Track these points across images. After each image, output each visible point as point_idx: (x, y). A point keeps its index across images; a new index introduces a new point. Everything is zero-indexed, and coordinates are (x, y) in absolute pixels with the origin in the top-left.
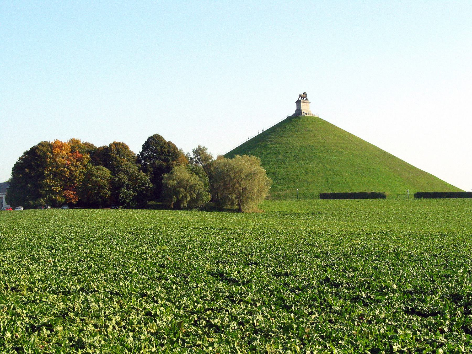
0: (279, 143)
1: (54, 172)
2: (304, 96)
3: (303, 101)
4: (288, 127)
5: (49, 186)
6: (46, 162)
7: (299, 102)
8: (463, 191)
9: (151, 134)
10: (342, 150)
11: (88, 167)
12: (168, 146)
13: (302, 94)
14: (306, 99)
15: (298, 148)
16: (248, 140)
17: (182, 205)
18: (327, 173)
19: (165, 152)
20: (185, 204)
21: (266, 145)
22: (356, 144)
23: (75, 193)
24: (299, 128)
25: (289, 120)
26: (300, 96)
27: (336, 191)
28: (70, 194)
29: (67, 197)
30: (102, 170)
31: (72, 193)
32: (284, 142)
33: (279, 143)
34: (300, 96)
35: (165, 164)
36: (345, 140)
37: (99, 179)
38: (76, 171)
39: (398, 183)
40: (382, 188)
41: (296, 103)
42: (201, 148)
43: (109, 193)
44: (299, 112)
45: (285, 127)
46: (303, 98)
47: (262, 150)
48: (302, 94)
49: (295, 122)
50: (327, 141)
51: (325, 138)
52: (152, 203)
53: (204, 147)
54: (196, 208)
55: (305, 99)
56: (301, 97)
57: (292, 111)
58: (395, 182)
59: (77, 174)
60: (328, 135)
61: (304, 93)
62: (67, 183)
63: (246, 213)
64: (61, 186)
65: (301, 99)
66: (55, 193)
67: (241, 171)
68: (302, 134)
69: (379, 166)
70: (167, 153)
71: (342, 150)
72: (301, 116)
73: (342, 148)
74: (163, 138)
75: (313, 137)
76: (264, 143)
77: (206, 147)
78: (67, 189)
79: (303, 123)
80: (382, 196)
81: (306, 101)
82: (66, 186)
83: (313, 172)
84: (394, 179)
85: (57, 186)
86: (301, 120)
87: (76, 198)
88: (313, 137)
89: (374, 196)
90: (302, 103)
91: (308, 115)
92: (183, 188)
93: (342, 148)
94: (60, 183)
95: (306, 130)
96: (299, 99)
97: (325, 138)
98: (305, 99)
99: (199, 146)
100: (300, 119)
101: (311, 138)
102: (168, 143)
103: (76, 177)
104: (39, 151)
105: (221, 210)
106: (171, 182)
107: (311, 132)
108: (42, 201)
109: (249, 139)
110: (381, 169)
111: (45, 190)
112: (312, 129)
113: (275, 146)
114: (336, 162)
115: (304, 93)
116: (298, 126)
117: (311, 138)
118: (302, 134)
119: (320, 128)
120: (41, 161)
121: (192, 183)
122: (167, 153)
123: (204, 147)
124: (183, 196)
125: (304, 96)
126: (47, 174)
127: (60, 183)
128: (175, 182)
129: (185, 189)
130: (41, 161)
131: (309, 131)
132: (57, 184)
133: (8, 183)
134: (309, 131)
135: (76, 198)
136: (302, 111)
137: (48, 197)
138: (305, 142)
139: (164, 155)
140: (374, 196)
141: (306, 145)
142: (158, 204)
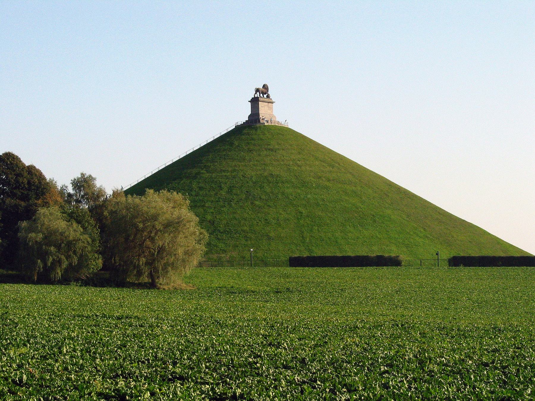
0: (221, 171)
2: (264, 90)
4: (236, 143)
7: (255, 102)
10: (328, 184)
12: (29, 174)
13: (261, 87)
14: (268, 97)
15: (254, 179)
17: (52, 276)
18: (302, 222)
19: (22, 183)
20: (59, 273)
21: (198, 173)
22: (351, 173)
24: (254, 145)
26: (257, 90)
27: (318, 252)
32: (230, 169)
33: (221, 171)
34: (257, 90)
35: (23, 204)
36: (333, 167)
39: (420, 240)
40: (394, 248)
41: (250, 103)
42: (86, 177)
45: (232, 144)
47: (191, 183)
48: (261, 87)
50: (303, 168)
54: (77, 280)
55: (265, 96)
56: (258, 93)
58: (417, 238)
60: (304, 157)
61: (265, 87)
63: (164, 289)
65: (258, 96)
67: (155, 217)
68: (259, 155)
69: (389, 212)
70: (27, 186)
71: (328, 184)
72: (258, 125)
73: (329, 180)
74: (19, 158)
75: (278, 161)
76: (195, 171)
77: (94, 176)
79: (261, 136)
80: (394, 262)
81: (267, 100)
83: (278, 220)
84: (415, 233)
86: (259, 132)
88: (278, 161)
90: (260, 103)
91: (270, 124)
92: (55, 246)
93: (329, 180)
95: (266, 149)
96: (256, 96)
97: (298, 162)
98: (265, 96)
99: (82, 174)
100: (256, 129)
101: (274, 163)
102: (28, 167)
105: (121, 284)
106: (33, 235)
107: (275, 151)
110: (392, 217)
112: (277, 147)
113: (214, 175)
114: (318, 205)
115: (265, 87)
116: (253, 142)
117: (274, 163)
118: (259, 155)
119: (291, 145)
121: (71, 238)
122: (27, 186)
123: (90, 176)
124: (54, 260)
125: (264, 90)
128: (41, 236)
129: (58, 247)
131: (272, 150)
134: (272, 150)
138: (265, 170)
139: (22, 189)
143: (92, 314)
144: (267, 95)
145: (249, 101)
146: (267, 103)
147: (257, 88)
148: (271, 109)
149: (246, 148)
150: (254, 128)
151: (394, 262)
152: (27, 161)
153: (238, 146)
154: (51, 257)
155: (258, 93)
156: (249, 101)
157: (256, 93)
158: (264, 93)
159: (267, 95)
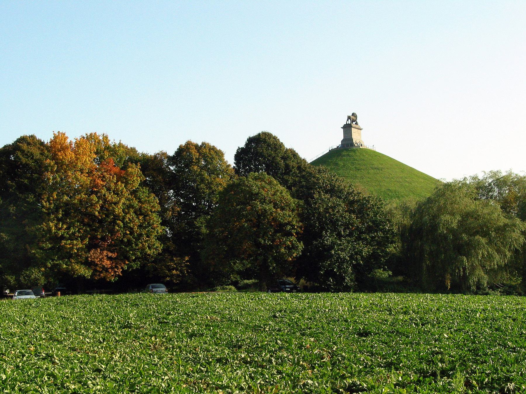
1: (67, 204)
2: (353, 118)
5: (56, 239)
6: (41, 180)
7: (347, 128)
9: (253, 133)
11: (140, 194)
13: (350, 115)
14: (356, 124)
23: (114, 255)
26: (349, 118)
28: (103, 258)
29: (97, 265)
30: (270, 183)
31: (107, 256)
37: (269, 207)
38: (116, 204)
43: (301, 246)
49: (348, 155)
51: (406, 179)
56: (349, 120)
59: (118, 210)
62: (96, 231)
64: (82, 239)
66: (69, 256)
77: (495, 170)
78: (96, 247)
81: (357, 126)
82: (93, 238)
85: (72, 237)
87: (116, 267)
90: (352, 128)
94: (79, 231)
96: (348, 123)
97: (406, 179)
98: (354, 123)
101: (386, 180)
103: (116, 217)
104: (23, 156)
107: (382, 170)
108: (36, 273)
111: (42, 248)
115: (353, 114)
117: (386, 180)
118: (369, 173)
120: (31, 179)
125: (353, 118)
126: (48, 209)
127: (79, 231)
130: (31, 179)
132: (73, 234)
133: (169, 156)
135: (116, 267)
136: (354, 141)
137: (49, 265)
141: (383, 189)
142: (247, 283)
143: (294, 319)
144: (355, 122)
145: (341, 128)
146: (357, 130)
147: (349, 115)
148: (360, 134)
149: (353, 167)
150: (351, 150)
152: (288, 145)
153: (344, 166)
154: (118, 222)
156: (341, 128)
157: (348, 120)
159: (355, 122)
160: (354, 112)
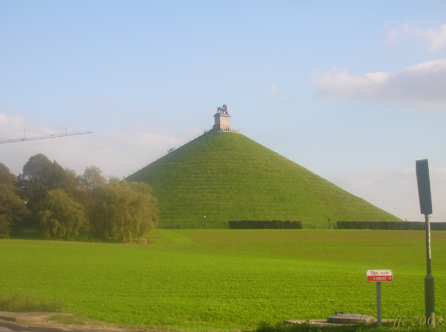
2: (224, 109)
3: (222, 115)
7: (217, 116)
8: (401, 221)
14: (227, 113)
16: (167, 153)
25: (206, 135)
34: (219, 109)
41: (214, 117)
44: (217, 126)
46: (222, 112)
48: (221, 106)
52: (31, 231)
53: (118, 178)
55: (225, 112)
56: (219, 110)
57: (209, 126)
61: (225, 106)
65: (220, 113)
80: (296, 225)
81: (226, 115)
89: (288, 225)
96: (218, 112)
98: (225, 112)
109: (168, 152)
115: (225, 106)
125: (224, 109)
140: (288, 225)
145: (214, 116)
151: (296, 225)
155: (219, 110)
156: (214, 116)
157: (218, 111)
158: (223, 111)
160: (217, 107)
